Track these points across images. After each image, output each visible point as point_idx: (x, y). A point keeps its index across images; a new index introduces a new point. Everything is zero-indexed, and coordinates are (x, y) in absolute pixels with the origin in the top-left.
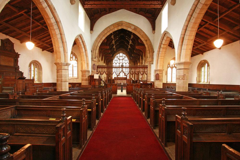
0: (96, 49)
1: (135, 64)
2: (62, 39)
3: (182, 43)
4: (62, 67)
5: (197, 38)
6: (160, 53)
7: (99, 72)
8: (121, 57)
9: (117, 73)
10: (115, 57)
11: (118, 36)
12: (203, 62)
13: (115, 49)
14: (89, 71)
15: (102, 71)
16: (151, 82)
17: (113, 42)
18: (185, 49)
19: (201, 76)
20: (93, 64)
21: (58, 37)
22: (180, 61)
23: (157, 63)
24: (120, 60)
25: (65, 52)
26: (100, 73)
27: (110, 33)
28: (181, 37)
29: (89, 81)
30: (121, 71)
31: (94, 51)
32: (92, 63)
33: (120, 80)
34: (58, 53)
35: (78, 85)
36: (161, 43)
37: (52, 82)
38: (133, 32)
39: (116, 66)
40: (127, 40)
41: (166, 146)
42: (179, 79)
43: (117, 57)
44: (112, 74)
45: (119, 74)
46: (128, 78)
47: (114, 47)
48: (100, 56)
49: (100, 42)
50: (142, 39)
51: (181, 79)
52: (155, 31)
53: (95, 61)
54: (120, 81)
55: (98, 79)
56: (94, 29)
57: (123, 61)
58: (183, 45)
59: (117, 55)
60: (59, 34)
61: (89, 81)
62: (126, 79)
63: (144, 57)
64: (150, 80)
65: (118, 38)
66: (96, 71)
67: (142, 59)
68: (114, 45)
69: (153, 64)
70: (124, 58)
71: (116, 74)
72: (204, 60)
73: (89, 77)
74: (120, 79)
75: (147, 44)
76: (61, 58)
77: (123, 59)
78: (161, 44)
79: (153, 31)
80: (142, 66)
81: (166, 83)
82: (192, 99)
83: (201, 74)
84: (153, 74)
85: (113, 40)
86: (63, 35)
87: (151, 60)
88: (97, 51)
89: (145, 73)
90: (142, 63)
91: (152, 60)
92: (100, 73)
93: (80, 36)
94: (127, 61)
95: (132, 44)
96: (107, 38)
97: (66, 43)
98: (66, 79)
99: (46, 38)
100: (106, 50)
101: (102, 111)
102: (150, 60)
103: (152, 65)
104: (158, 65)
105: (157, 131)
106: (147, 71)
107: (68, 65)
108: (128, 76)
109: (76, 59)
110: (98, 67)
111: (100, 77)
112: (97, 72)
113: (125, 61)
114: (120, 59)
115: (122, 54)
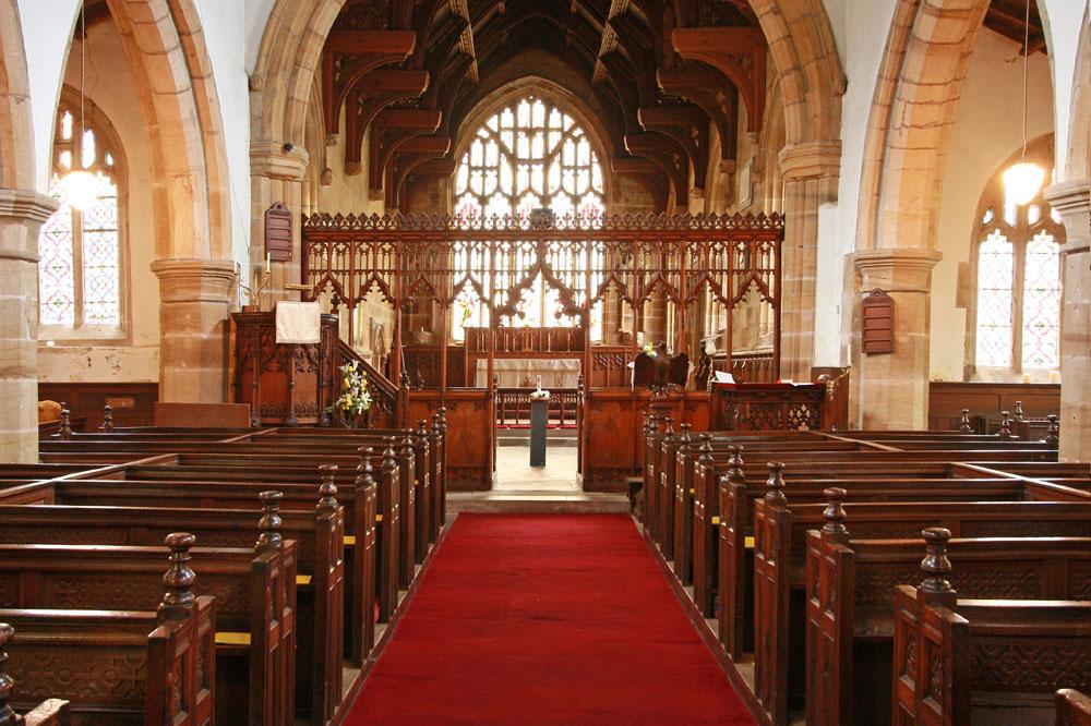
0: (297, 63)
1: (661, 205)
6: (907, 91)
8: (530, 132)
9: (493, 292)
10: (474, 136)
13: (475, 64)
14: (227, 276)
16: (816, 371)
20: (265, 206)
23: (878, 194)
24: (523, 169)
31: (280, 83)
39: (483, 218)
44: (446, 303)
45: (515, 294)
46: (596, 335)
47: (467, 41)
48: (331, 129)
53: (284, 178)
54: (518, 363)
55: (313, 351)
59: (492, 123)
61: (226, 365)
62: (574, 343)
63: (745, 137)
66: (295, 267)
67: (730, 152)
70: (559, 149)
71: (487, 295)
73: (226, 324)
75: (777, 11)
77: (547, 160)
80: (725, 217)
81: (959, 379)
84: (838, 300)
87: (817, 161)
88: (306, 84)
89: (763, 289)
90: (730, 195)
100: (385, 67)
106: (778, 272)
108: (596, 314)
109: (110, 160)
110: (318, 233)
111: (328, 326)
112: (304, 281)
114: (523, 154)
115: (539, 107)
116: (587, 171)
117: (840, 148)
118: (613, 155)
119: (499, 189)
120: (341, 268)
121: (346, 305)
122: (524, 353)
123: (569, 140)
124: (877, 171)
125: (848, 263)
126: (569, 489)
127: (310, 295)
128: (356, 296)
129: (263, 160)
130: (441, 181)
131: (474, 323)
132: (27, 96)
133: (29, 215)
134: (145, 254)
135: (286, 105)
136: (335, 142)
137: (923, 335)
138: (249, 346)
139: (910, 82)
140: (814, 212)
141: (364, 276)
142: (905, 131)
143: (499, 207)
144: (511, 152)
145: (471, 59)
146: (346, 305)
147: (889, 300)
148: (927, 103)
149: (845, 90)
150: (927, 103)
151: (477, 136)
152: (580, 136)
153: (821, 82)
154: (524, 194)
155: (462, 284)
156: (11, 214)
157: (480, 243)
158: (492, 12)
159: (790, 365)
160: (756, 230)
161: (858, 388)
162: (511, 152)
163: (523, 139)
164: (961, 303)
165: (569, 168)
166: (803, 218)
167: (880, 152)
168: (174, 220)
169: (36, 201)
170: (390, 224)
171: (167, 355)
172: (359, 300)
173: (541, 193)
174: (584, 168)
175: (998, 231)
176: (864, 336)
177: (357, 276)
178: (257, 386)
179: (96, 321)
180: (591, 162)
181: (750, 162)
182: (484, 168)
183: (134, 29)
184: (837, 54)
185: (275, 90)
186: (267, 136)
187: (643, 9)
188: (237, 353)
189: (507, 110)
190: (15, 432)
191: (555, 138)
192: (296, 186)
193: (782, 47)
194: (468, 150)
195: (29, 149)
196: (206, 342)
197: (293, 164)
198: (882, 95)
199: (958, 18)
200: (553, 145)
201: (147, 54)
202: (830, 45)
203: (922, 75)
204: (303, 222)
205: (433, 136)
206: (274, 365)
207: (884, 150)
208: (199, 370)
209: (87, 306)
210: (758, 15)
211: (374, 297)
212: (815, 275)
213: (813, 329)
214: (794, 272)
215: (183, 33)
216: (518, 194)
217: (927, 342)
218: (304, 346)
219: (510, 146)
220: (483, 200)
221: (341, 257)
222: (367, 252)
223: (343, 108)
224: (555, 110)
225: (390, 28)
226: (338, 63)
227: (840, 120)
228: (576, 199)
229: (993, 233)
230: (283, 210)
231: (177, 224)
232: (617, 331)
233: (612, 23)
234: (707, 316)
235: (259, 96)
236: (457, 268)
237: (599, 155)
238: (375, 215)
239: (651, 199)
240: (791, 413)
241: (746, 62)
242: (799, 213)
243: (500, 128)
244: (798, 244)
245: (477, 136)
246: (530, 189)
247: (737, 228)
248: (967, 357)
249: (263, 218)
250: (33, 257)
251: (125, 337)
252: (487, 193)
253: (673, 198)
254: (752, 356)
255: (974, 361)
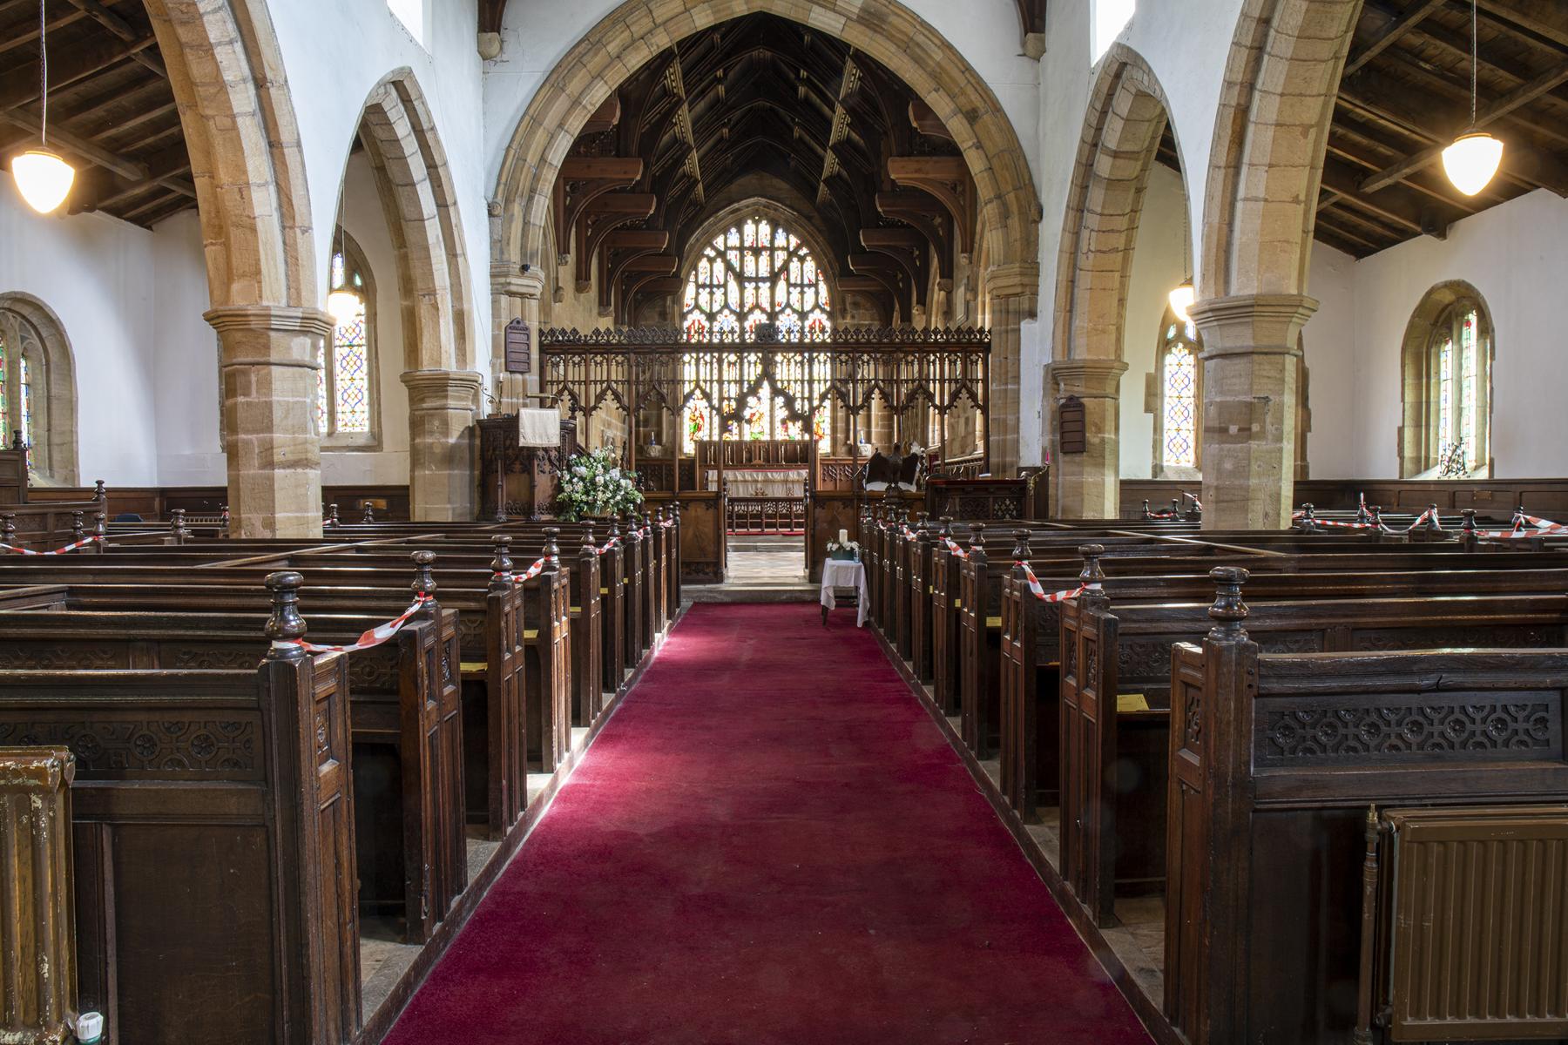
0: (533, 191)
1: (887, 320)
2: (271, 126)
3: (1233, 155)
4: (267, 347)
5: (1370, 99)
6: (1092, 221)
7: (560, 393)
8: (757, 251)
9: (721, 399)
10: (700, 256)
11: (720, 73)
12: (1448, 297)
13: (700, 186)
14: (471, 385)
15: (587, 382)
16: (1020, 470)
17: (684, 119)
18: (1256, 200)
19: (1438, 411)
20: (505, 321)
21: (234, 103)
22: (1227, 293)
23: (1071, 311)
24: (750, 287)
25: (292, 228)
26: (572, 394)
27: (655, 51)
28: (1223, 106)
29: (477, 473)
30: (758, 383)
31: (517, 209)
32: (496, 313)
33: (749, 464)
34: (235, 234)
35: (382, 504)
36: (1089, 139)
37: (155, 484)
38: (859, 38)
39: (711, 332)
40: (807, 99)
41: (1108, 917)
42: (1223, 430)
43: (722, 254)
44: (676, 411)
45: (741, 401)
46: (824, 447)
47: (693, 163)
48: (563, 250)
49: (561, 126)
50: (940, 104)
51: (1233, 429)
52: (1043, 41)
53: (522, 296)
54: (748, 475)
55: (553, 454)
56: (510, 16)
57: (772, 289)
58: (1244, 170)
59: (719, 242)
60: (244, 80)
61: (472, 467)
62: (801, 455)
63: (961, 259)
64: (1008, 459)
65: (721, 89)
66: (533, 378)
67: (948, 272)
68: (690, 149)
69: (1032, 314)
70: (785, 267)
71: (715, 402)
72: (1451, 285)
73: (471, 430)
74: (750, 460)
75: (979, 146)
76: (258, 272)
77: (773, 278)
78: (1095, 145)
79: (1030, 35)
80: (947, 331)
81: (1148, 476)
82: (1252, 556)
83: (1438, 403)
84: (1038, 406)
85: (679, 103)
86: (272, 91)
87: (1017, 280)
88: (542, 206)
89: (973, 396)
90: (948, 313)
91: (1026, 280)
92: (572, 394)
93: (401, 86)
94: (810, 292)
95: (853, 135)
96: (623, 93)
97: (301, 152)
98: (305, 442)
99: (111, 104)
100: (614, 191)
101: (608, 686)
102: (1010, 281)
103: (1025, 325)
104: (1077, 323)
105: (1045, 836)
106: (985, 381)
107: (314, 326)
108: (823, 420)
109: (358, 281)
110: (557, 346)
111: (567, 431)
112: (542, 390)
113: (795, 292)
114: (750, 270)
115: (765, 228)
116: (813, 289)
117: (1038, 269)
118: (836, 271)
119: (726, 306)
120: (577, 379)
121: (582, 413)
122: (754, 465)
123: (795, 259)
124: (1069, 290)
125: (1046, 373)
126: (796, 580)
127: (549, 402)
128: (592, 404)
129: (502, 280)
130: (669, 299)
131: (704, 435)
132: (311, 228)
133: (313, 330)
134: (394, 365)
135: (523, 229)
136: (567, 262)
137: (1113, 437)
138: (494, 450)
139: (1093, 212)
140: (1017, 327)
141: (599, 386)
142: (1091, 256)
143: (727, 321)
144: (738, 270)
145: (696, 182)
146: (582, 413)
147: (1082, 405)
148: (1108, 231)
149: (1041, 218)
150: (1108, 231)
151: (703, 256)
152: (806, 255)
153: (1019, 210)
154: (751, 311)
155: (691, 393)
156: (297, 328)
157: (709, 355)
158: (716, 136)
159: (998, 465)
160: (898, 343)
161: (1057, 484)
162: (738, 270)
163: (749, 259)
164: (1149, 408)
165: (795, 285)
166: (1007, 332)
167: (1070, 274)
168: (421, 335)
169: (319, 317)
170: (871, 337)
171: (417, 457)
172: (595, 408)
173: (769, 310)
174: (810, 286)
175: (1180, 345)
176: (1062, 438)
177: (593, 386)
178: (502, 486)
179: (348, 430)
180: (817, 280)
181: (965, 281)
182: (711, 286)
183: (386, 164)
184: (1033, 186)
185: (513, 215)
186: (506, 257)
187: (861, 136)
188: (482, 457)
189: (733, 230)
190: (306, 515)
191: (781, 257)
192: (534, 304)
193: (984, 178)
194: (696, 269)
195: (313, 273)
196: (453, 446)
197: (531, 282)
198: (1070, 224)
199: (1130, 159)
200: (778, 264)
201: (398, 185)
202: (1027, 177)
203: (1103, 207)
204: (540, 337)
205: (660, 255)
206: (517, 467)
207: (1074, 272)
208: (447, 472)
209: (339, 416)
210: (962, 150)
211: (610, 403)
212: (1019, 383)
213: (1018, 433)
214: (1000, 381)
215: (432, 167)
216: (738, 310)
217: (1117, 443)
218: (546, 450)
219: (737, 265)
220: (711, 317)
221: (577, 368)
222: (601, 363)
223: (574, 229)
224: (780, 231)
225: (617, 155)
226: (568, 188)
227: (1037, 245)
228: (803, 316)
229: (1176, 346)
230: (521, 325)
231: (425, 340)
232: (846, 444)
233: (834, 148)
234: (931, 427)
235: (498, 221)
236: (686, 378)
237: (825, 273)
238: (608, 329)
239: (876, 316)
240: (996, 507)
241: (959, 189)
242: (1003, 327)
243: (727, 248)
244: (1002, 356)
245: (703, 256)
246: (757, 306)
247: (857, 341)
248: (1155, 457)
249: (503, 333)
250: (314, 365)
251: (376, 443)
252: (714, 310)
253: (896, 315)
254: (969, 461)
255: (1162, 461)
